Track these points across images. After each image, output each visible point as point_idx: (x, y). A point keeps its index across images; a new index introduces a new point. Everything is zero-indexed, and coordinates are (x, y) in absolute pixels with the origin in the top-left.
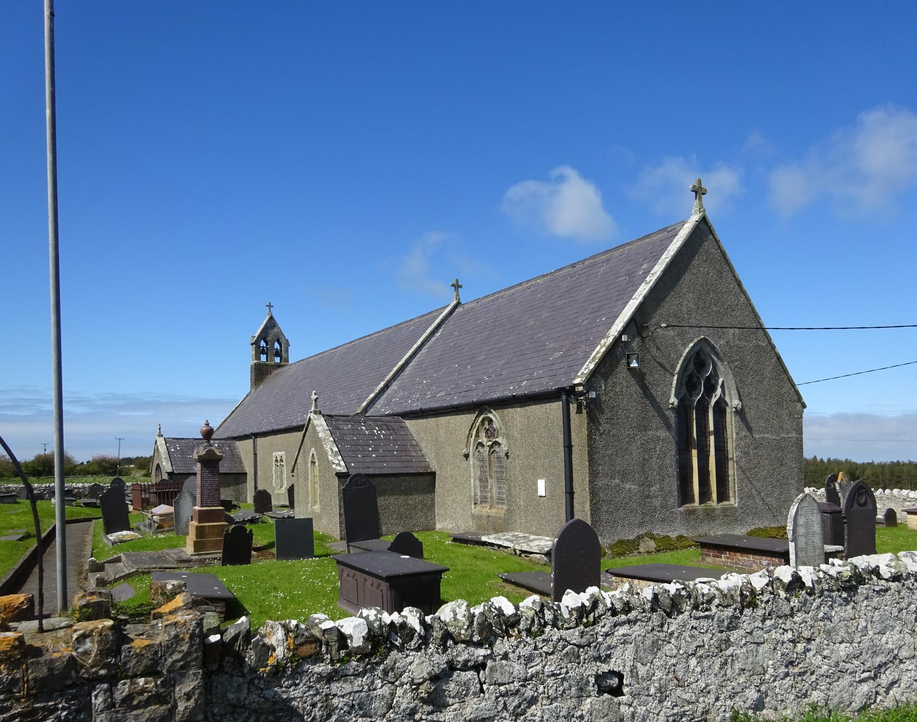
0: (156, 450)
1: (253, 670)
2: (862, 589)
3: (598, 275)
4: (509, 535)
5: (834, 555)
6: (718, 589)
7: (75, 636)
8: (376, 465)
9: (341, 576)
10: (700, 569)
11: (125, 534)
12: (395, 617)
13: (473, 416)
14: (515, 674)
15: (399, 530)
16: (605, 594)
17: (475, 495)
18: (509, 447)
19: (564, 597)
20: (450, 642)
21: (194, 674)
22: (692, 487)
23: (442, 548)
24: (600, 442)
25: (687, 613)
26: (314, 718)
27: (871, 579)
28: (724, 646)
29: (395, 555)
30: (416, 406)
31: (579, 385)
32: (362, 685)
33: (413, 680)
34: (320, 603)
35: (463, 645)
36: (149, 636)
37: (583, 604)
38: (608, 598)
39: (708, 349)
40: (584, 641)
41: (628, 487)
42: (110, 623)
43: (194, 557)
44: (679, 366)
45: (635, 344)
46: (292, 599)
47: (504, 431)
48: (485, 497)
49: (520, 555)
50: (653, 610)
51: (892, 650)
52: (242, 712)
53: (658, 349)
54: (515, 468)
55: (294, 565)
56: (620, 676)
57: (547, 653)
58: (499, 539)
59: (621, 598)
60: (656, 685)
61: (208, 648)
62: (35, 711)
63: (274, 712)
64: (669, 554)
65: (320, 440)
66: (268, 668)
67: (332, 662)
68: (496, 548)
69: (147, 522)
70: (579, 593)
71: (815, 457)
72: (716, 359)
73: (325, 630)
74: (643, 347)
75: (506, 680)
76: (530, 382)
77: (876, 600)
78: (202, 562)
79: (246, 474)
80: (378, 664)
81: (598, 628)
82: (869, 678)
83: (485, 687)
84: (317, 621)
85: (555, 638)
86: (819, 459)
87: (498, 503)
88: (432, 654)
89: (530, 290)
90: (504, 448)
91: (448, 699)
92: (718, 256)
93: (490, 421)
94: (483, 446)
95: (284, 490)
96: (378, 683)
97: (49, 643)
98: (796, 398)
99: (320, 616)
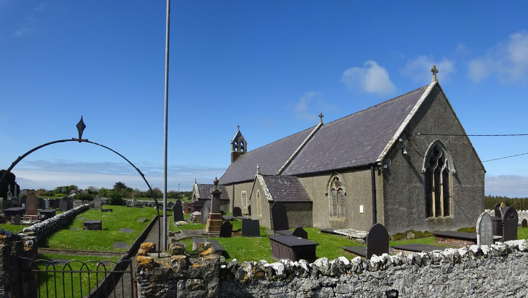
0: (194, 189)
2: (510, 256)
3: (390, 109)
4: (346, 230)
5: (498, 240)
6: (443, 255)
7: (172, 261)
8: (286, 197)
9: (272, 245)
10: (435, 246)
11: (182, 222)
14: (350, 289)
15: (297, 226)
16: (391, 257)
17: (331, 212)
19: (372, 258)
20: (320, 275)
22: (432, 209)
24: (389, 189)
25: (428, 266)
27: (514, 251)
28: (445, 280)
30: (303, 172)
31: (379, 162)
37: (380, 261)
38: (392, 258)
39: (440, 145)
40: (381, 276)
41: (402, 209)
42: (185, 257)
44: (426, 153)
45: (405, 143)
46: (248, 253)
47: (344, 183)
48: (336, 213)
50: (413, 264)
51: (523, 282)
53: (416, 145)
56: (397, 292)
62: (157, 287)
69: (190, 218)
71: (490, 196)
73: (266, 267)
74: (409, 144)
77: (516, 260)
78: (212, 235)
80: (289, 282)
81: (387, 271)
82: (512, 294)
83: (336, 294)
85: (367, 275)
86: (492, 196)
90: (344, 191)
92: (444, 102)
93: (338, 179)
94: (334, 190)
95: (246, 207)
96: (289, 290)
97: (162, 262)
98: (481, 168)
99: (263, 261)
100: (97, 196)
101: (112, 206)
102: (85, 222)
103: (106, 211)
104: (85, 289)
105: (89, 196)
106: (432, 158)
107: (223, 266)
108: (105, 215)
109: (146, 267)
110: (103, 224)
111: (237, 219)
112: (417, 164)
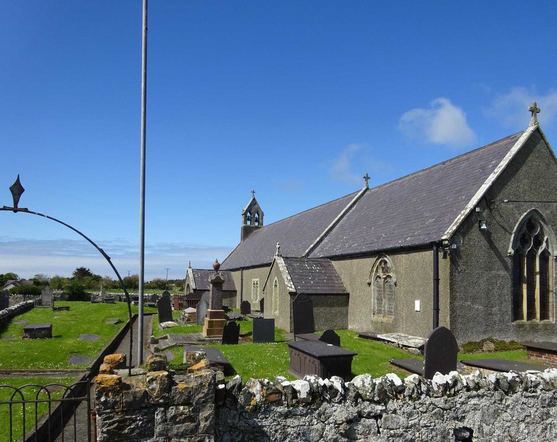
0: (187, 276)
1: (243, 407)
3: (467, 166)
6: (542, 378)
7: (148, 380)
8: (313, 288)
9: (291, 354)
12: (326, 382)
13: (375, 259)
14: (401, 423)
15: (326, 328)
17: (374, 308)
18: (397, 279)
19: (435, 377)
21: (210, 406)
23: (352, 341)
26: (276, 439)
28: (545, 417)
29: (323, 344)
30: (339, 253)
31: (445, 240)
32: (305, 422)
33: (336, 421)
34: (278, 370)
35: (368, 403)
36: (186, 383)
37: (447, 382)
38: (464, 379)
39: (537, 217)
40: (447, 406)
41: (476, 307)
42: (166, 373)
43: (206, 339)
44: (516, 228)
45: (485, 214)
46: (262, 366)
47: (394, 269)
48: (380, 310)
49: (402, 348)
50: (495, 389)
52: (235, 431)
53: (501, 216)
54: (401, 293)
55: (263, 346)
56: (471, 431)
57: (422, 412)
58: (389, 337)
59: (474, 380)
60: (496, 439)
61: (218, 392)
62: (125, 420)
63: (253, 433)
64: (504, 353)
65: (280, 272)
66: (251, 407)
67: (288, 406)
68: (386, 342)
69: (182, 317)
70: (444, 375)
72: (542, 223)
73: (284, 387)
74: (491, 216)
75: (394, 427)
76: (413, 238)
78: (211, 341)
79: (236, 291)
80: (315, 409)
81: (457, 399)
83: (381, 430)
84: (280, 381)
85: (427, 403)
87: (389, 314)
88: (348, 406)
89: (414, 180)
91: (357, 435)
94: (380, 278)
95: (258, 302)
96: (315, 421)
97: (134, 382)
100: (47, 288)
101: (69, 302)
102: (25, 328)
103: (60, 309)
104: (17, 428)
105: (35, 288)
106: (524, 235)
107: (221, 386)
108: (57, 317)
109: (110, 391)
110: (54, 329)
111: (247, 318)
112: (501, 243)
